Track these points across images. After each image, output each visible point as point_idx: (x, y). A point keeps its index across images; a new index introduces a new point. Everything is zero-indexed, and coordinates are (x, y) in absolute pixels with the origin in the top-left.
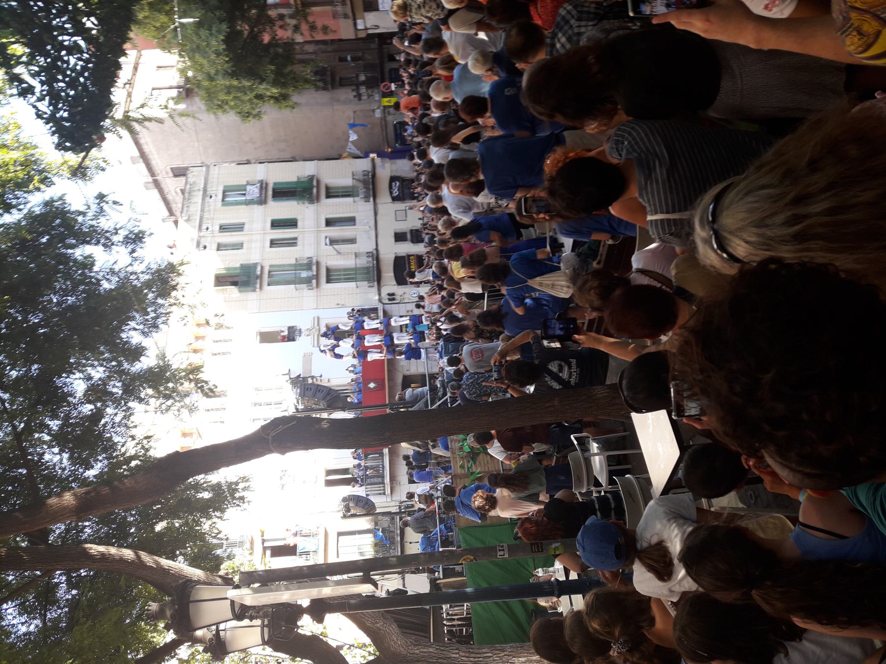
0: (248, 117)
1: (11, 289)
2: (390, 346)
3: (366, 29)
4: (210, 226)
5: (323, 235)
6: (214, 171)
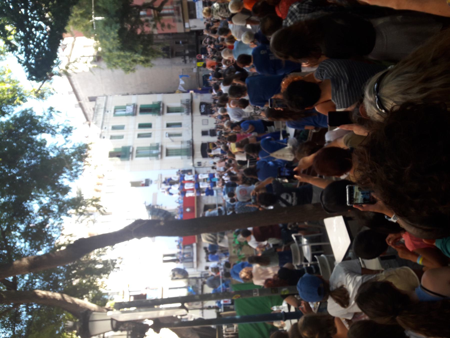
0: (128, 71)
1: (3, 156)
2: (198, 190)
3: (190, 28)
4: (107, 126)
5: (165, 132)
6: (110, 99)
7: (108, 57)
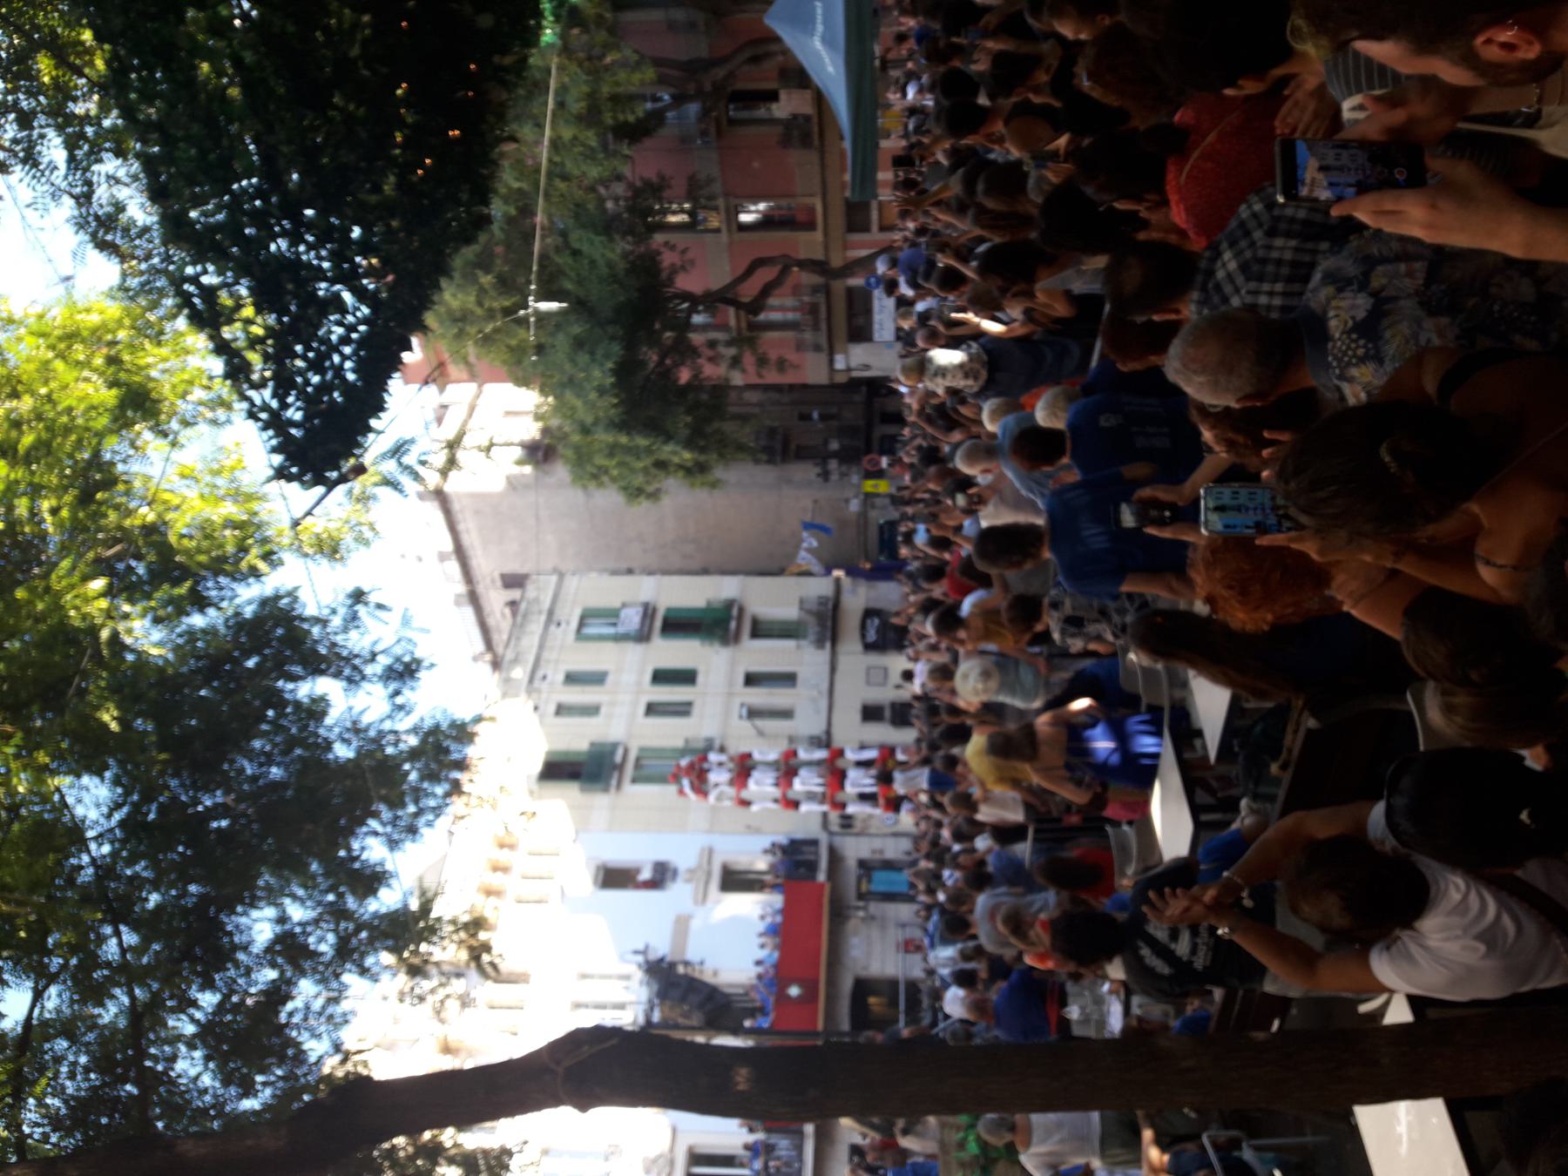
3: (849, 370)
5: (737, 701)
6: (572, 583)
7: (577, 449)
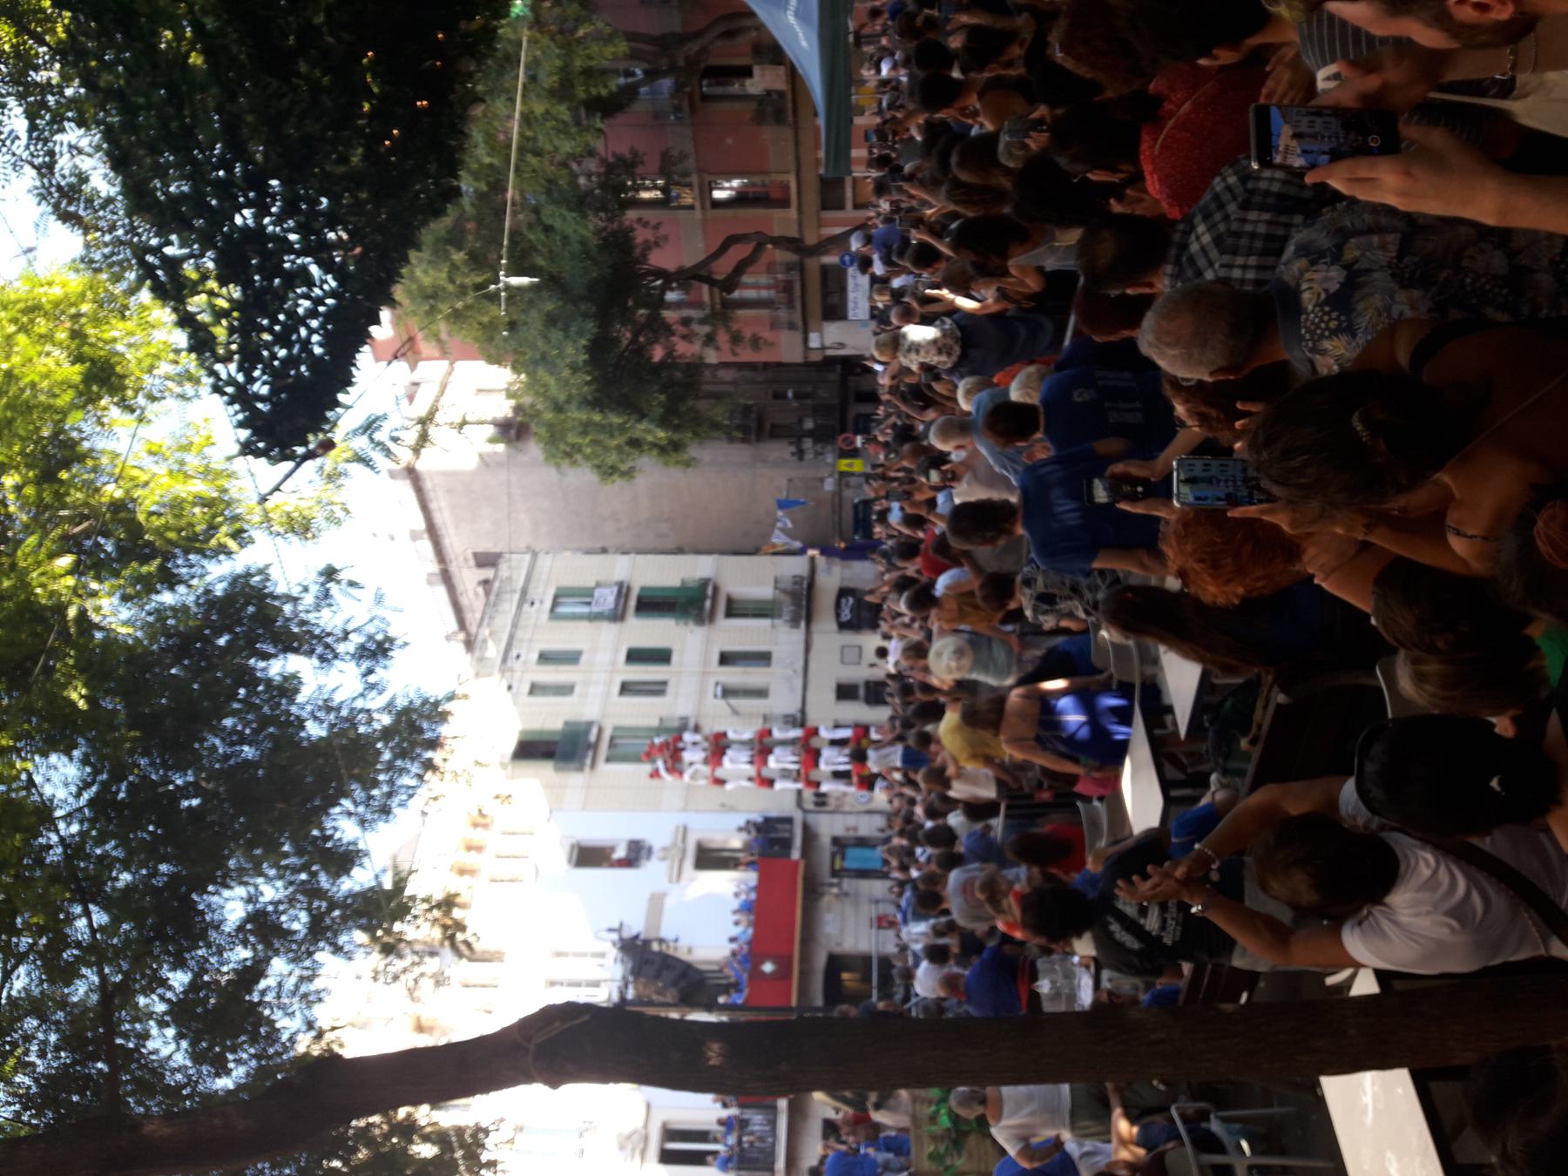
3: (823, 348)
5: (712, 681)
6: (545, 562)
